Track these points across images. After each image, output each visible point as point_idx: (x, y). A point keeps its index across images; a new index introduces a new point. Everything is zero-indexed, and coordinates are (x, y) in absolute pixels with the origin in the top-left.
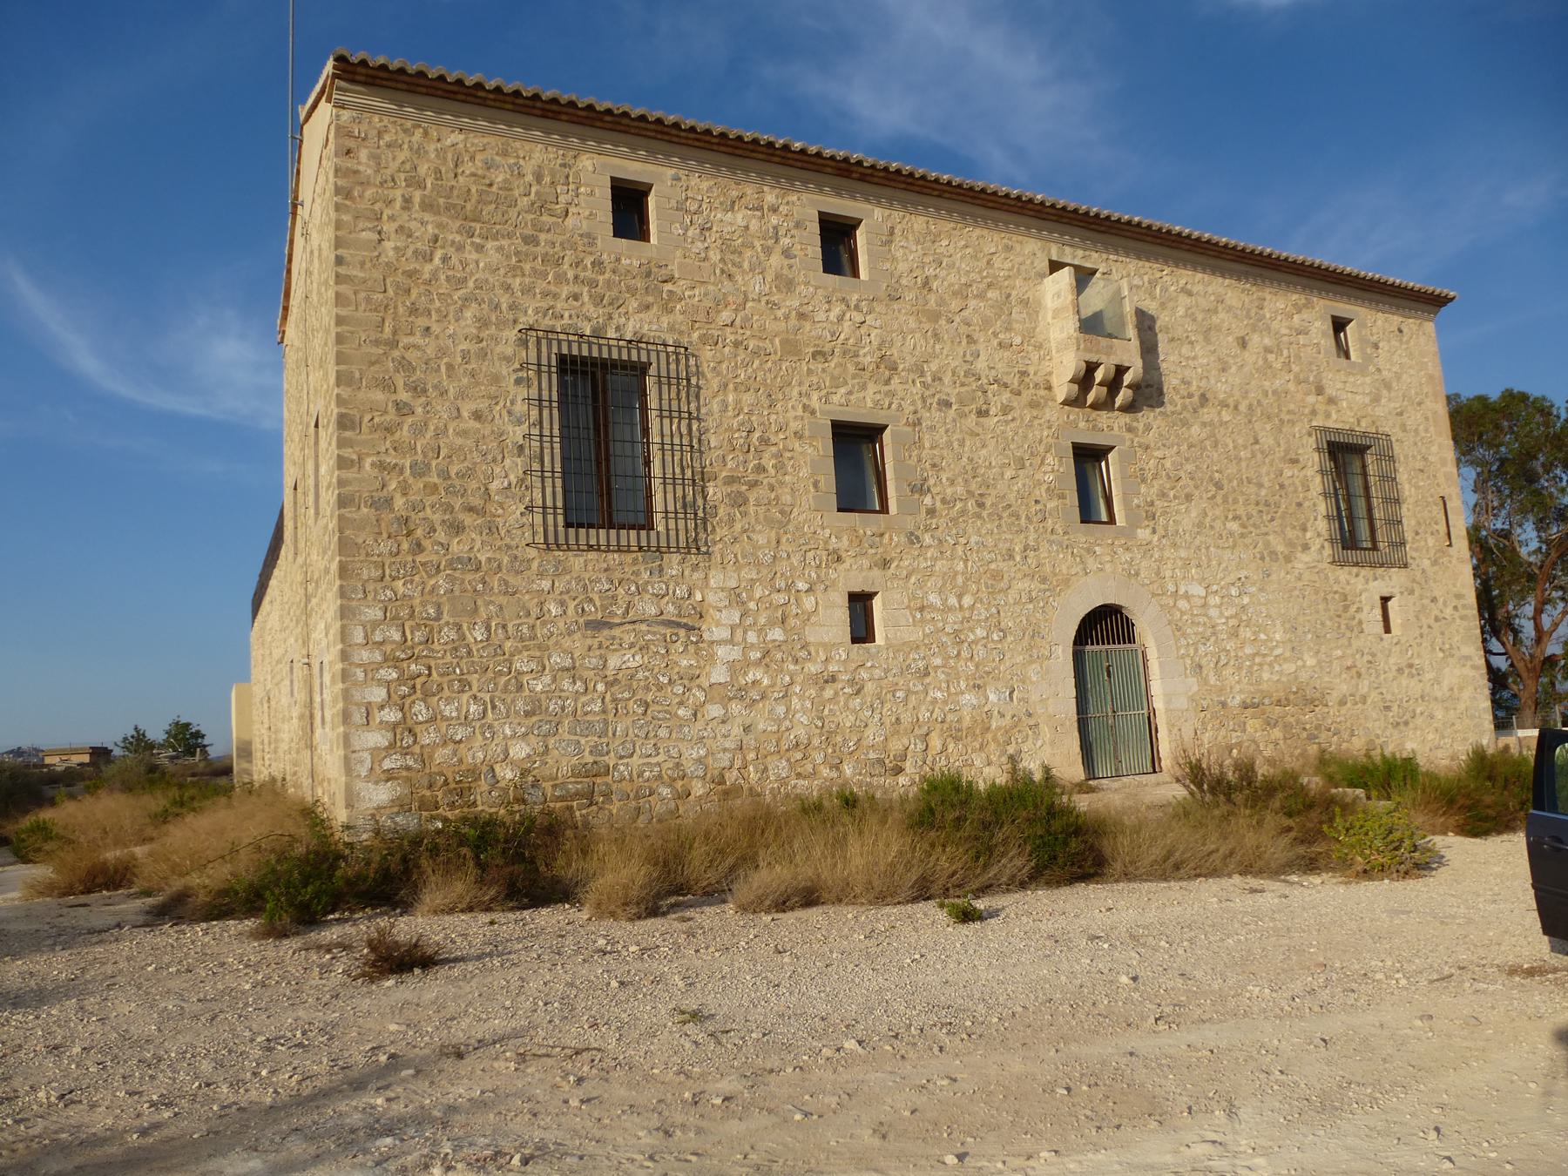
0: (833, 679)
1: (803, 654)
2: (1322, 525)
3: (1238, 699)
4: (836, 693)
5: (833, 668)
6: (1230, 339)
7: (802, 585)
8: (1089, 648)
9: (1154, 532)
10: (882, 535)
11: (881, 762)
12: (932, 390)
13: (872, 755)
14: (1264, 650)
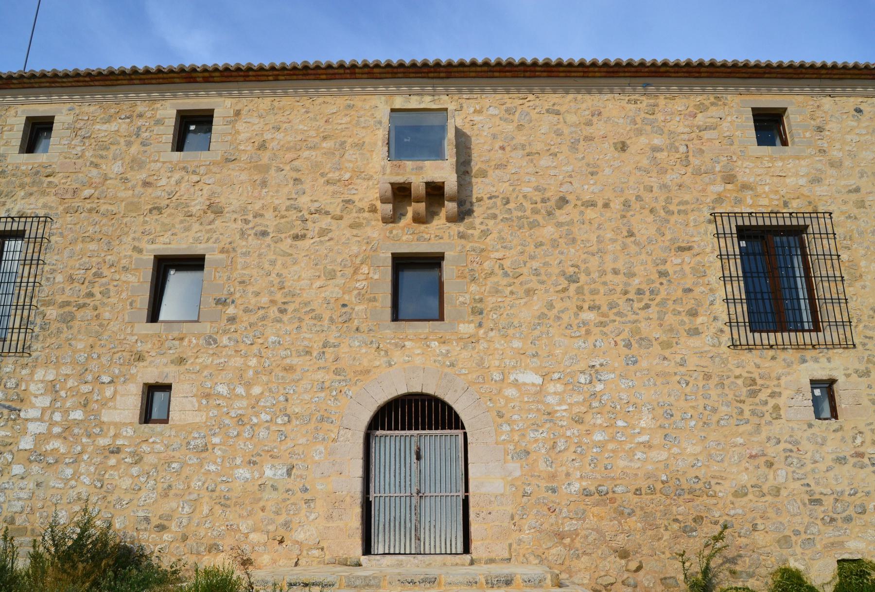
0: (117, 451)
1: (97, 430)
2: (721, 310)
3: (576, 486)
4: (118, 462)
5: (119, 442)
6: (606, 145)
7: (106, 379)
8: (379, 432)
9: (480, 325)
10: (182, 339)
11: (147, 519)
12: (251, 225)
13: (141, 514)
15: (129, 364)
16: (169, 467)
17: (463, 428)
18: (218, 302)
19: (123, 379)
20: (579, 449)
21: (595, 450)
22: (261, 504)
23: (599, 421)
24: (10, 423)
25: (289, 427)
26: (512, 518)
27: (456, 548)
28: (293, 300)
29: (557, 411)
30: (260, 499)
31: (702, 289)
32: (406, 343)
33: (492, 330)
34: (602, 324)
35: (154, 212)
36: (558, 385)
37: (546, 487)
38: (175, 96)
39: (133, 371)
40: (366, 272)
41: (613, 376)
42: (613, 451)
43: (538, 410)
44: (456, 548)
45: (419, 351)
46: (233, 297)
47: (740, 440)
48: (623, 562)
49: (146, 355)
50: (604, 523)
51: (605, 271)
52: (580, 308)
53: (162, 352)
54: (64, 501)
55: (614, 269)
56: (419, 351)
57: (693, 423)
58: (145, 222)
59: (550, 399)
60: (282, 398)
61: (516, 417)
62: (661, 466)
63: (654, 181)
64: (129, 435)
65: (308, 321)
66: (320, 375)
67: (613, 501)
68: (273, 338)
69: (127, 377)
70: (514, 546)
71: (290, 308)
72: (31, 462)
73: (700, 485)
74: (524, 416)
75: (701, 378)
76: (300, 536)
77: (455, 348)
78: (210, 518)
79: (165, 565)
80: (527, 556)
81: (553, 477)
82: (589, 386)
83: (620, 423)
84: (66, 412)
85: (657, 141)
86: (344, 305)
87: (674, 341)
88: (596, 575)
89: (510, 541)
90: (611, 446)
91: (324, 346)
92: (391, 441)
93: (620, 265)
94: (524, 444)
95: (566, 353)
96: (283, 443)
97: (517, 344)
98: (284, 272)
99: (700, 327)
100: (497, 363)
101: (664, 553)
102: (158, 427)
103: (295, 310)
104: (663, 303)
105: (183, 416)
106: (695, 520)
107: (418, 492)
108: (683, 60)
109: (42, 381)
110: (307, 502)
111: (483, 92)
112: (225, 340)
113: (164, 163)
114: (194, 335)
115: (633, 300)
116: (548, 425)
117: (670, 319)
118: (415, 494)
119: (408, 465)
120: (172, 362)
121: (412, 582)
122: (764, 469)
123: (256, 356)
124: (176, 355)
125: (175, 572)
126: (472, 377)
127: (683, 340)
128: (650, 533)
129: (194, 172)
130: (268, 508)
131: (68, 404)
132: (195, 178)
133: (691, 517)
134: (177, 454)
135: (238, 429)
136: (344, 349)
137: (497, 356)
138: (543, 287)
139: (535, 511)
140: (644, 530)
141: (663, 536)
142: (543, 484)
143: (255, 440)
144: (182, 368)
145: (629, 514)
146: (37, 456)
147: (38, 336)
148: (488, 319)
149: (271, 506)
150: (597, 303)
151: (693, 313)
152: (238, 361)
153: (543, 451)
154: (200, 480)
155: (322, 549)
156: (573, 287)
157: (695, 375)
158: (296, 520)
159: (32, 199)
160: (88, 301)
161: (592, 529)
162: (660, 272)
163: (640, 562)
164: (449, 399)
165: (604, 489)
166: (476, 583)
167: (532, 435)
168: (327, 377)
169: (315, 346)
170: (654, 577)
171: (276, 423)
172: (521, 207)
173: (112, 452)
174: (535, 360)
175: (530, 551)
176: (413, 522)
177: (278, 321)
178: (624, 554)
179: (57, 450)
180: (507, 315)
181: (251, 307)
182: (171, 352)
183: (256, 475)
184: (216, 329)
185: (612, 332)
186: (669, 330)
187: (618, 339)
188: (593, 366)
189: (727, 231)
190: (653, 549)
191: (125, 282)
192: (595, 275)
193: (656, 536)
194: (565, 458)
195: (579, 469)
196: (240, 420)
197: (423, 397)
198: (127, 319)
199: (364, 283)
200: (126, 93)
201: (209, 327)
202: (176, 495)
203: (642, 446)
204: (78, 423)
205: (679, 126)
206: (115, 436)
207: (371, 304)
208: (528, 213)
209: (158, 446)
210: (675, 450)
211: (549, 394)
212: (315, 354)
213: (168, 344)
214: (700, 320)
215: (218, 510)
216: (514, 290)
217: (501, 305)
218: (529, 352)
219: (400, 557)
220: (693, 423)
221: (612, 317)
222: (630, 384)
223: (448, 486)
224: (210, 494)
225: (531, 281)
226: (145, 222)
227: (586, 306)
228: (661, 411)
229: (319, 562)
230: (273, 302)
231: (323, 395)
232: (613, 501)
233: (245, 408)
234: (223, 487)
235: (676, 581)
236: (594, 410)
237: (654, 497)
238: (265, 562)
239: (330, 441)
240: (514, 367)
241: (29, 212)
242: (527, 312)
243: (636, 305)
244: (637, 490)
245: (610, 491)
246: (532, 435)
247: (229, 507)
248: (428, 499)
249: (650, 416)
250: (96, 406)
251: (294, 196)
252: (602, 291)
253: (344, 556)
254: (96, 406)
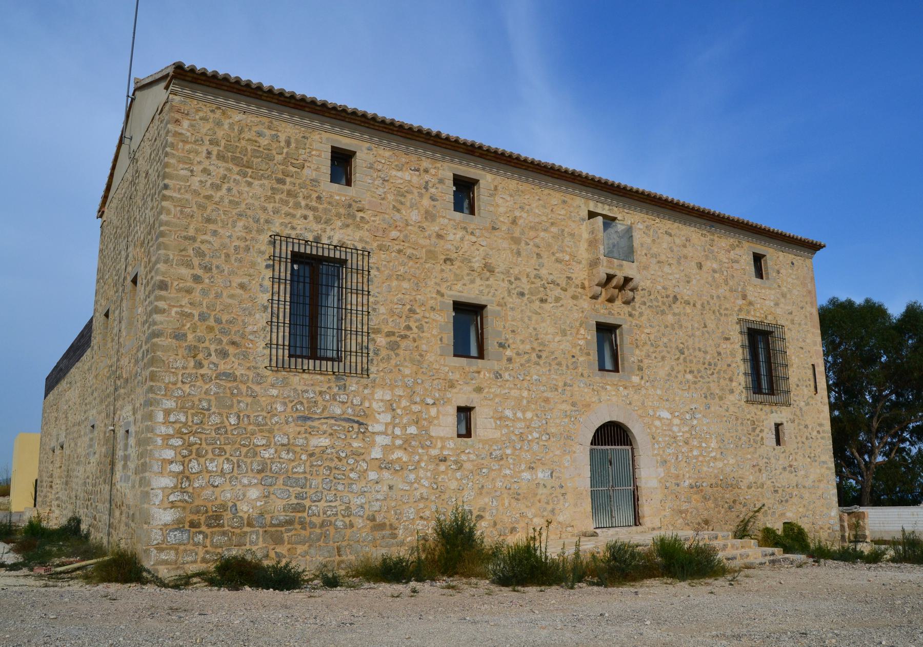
0: (444, 460)
3: (687, 483)
5: (446, 453)
10: (479, 372)
24: (361, 436)
35: (448, 262)
38: (452, 161)
39: (449, 395)
47: (749, 456)
54: (412, 500)
58: (442, 270)
60: (544, 422)
63: (714, 293)
68: (535, 377)
71: (544, 355)
72: (382, 469)
76: (561, 518)
77: (631, 391)
84: (404, 428)
85: (715, 266)
86: (573, 357)
97: (659, 392)
108: (434, 130)
109: (382, 401)
110: (563, 495)
111: (635, 210)
113: (450, 220)
122: (758, 474)
127: (727, 396)
129: (472, 233)
131: (405, 421)
132: (474, 239)
146: (384, 465)
147: (372, 360)
152: (515, 393)
156: (682, 357)
159: (349, 231)
160: (408, 333)
172: (656, 299)
173: (441, 461)
179: (399, 459)
189: (284, 255)
196: (521, 437)
200: (416, 148)
204: (413, 437)
205: (723, 256)
206: (443, 448)
208: (660, 304)
210: (725, 462)
212: (560, 390)
219: (617, 529)
226: (442, 270)
230: (533, 349)
231: (566, 420)
241: (349, 244)
250: (425, 423)
251: (537, 267)
254: (425, 423)
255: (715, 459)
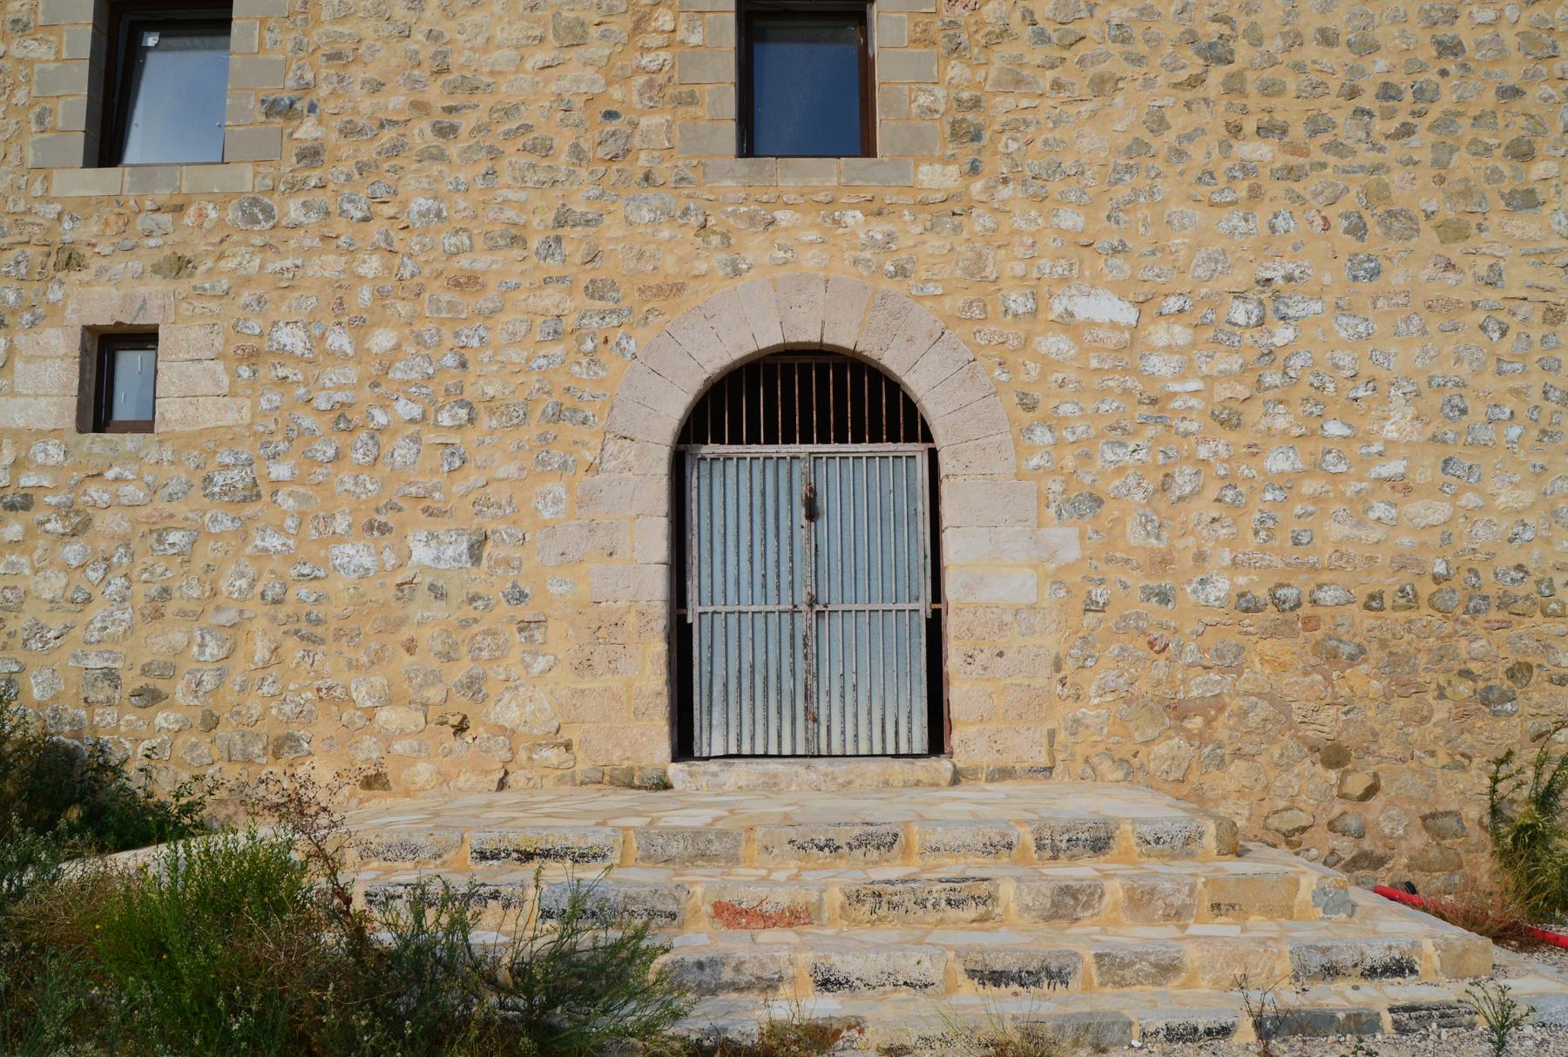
3: (1221, 587)
4: (28, 531)
5: (28, 480)
9: (974, 169)
10: (179, 209)
11: (111, 676)
13: (95, 662)
14: (1332, 463)
15: (44, 278)
16: (160, 541)
17: (928, 437)
18: (273, 108)
19: (27, 317)
20: (1230, 493)
21: (1269, 496)
22: (405, 633)
23: (1281, 423)
25: (472, 435)
26: (1058, 667)
27: (910, 741)
28: (474, 100)
29: (1175, 394)
30: (401, 622)
31: (1546, 89)
32: (779, 214)
33: (1005, 181)
34: (1292, 173)
36: (1177, 329)
37: (1144, 589)
39: (55, 294)
40: (669, 26)
41: (1317, 307)
42: (1315, 499)
43: (1126, 392)
44: (910, 741)
45: (813, 235)
46: (314, 98)
48: (1333, 775)
49: (88, 252)
50: (1288, 678)
51: (1298, 35)
52: (1236, 130)
53: (128, 244)
55: (1322, 31)
56: (813, 235)
57: (1515, 432)
59: (1158, 365)
60: (450, 360)
61: (1067, 409)
62: (1434, 538)
64: (51, 462)
65: (513, 157)
66: (550, 299)
67: (1311, 623)
68: (420, 203)
69: (39, 311)
70: (1062, 736)
71: (466, 122)
73: (1528, 587)
74: (1090, 408)
75: (1537, 318)
76: (509, 714)
77: (909, 228)
78: (275, 671)
79: (163, 790)
80: (1095, 760)
81: (1164, 561)
82: (1256, 332)
83: (1334, 428)
86: (610, 115)
87: (1473, 221)
88: (1266, 807)
89: (1051, 725)
90: (1309, 487)
91: (560, 223)
92: (741, 474)
93: (1338, 21)
94: (1088, 480)
95: (1199, 245)
96: (457, 475)
97: (1070, 219)
98: (448, 28)
99: (1539, 188)
100: (1019, 269)
101: (1432, 754)
102: (129, 441)
103: (478, 129)
104: (1446, 123)
105: (191, 410)
106: (1511, 674)
107: (813, 601)
110: (524, 626)
112: (293, 210)
114: (212, 197)
115: (1370, 114)
116: (1150, 431)
117: (1464, 164)
118: (803, 607)
119: (784, 534)
120: (156, 269)
121: (831, 847)
123: (377, 249)
124: (167, 252)
125: (188, 809)
126: (950, 304)
127: (1494, 219)
128: (1400, 704)
130: (422, 645)
133: (1502, 667)
134: (179, 509)
135: (339, 440)
136: (612, 228)
137: (1019, 252)
138: (1138, 72)
139: (1115, 649)
140: (1387, 697)
141: (1431, 711)
142: (1137, 580)
143: (383, 469)
144: (183, 286)
145: (1352, 658)
148: (995, 153)
149: (430, 639)
150: (1279, 117)
151: (1523, 153)
152: (329, 265)
153: (1138, 497)
154: (242, 575)
155: (568, 746)
156: (1217, 74)
157: (1524, 309)
158: (497, 672)
161: (1259, 695)
162: (1439, 43)
163: (1375, 775)
164: (893, 360)
165: (1290, 593)
166: (1009, 846)
167: (1110, 456)
168: (569, 304)
169: (535, 221)
170: (1406, 813)
171: (437, 425)
173: (12, 507)
174: (1118, 261)
175: (1101, 748)
176: (800, 676)
177: (433, 158)
178: (1335, 757)
180: (1046, 142)
181: (361, 122)
182: (152, 242)
183: (390, 559)
184: (269, 182)
185: (1316, 195)
186: (1460, 194)
187: (1330, 212)
188: (1268, 280)
190: (1408, 745)
191: (20, 60)
192: (1274, 45)
193: (1415, 711)
194: (1194, 516)
195: (1229, 542)
197: (822, 360)
198: (30, 160)
199: (663, 55)
201: (249, 176)
202: (183, 614)
203: (1387, 486)
207: (681, 111)
209: (131, 488)
210: (1470, 499)
211: (1153, 350)
212: (534, 244)
213: (143, 222)
214: (1538, 169)
215: (294, 650)
216: (1064, 79)
217: (1029, 116)
218: (1103, 243)
220: (1515, 432)
221: (1318, 155)
222: (1361, 328)
223: (890, 586)
224: (271, 609)
225: (1109, 55)
227: (1250, 125)
228: (1435, 400)
229: (561, 780)
230: (420, 107)
231: (558, 350)
232: (1311, 623)
233: (354, 387)
234: (303, 593)
235: (1459, 821)
236: (1270, 395)
237: (1413, 615)
238: (420, 780)
239: (581, 472)
240: (1064, 280)
242: (1095, 139)
243: (1379, 126)
244: (1372, 597)
245: (1305, 599)
246: (1110, 456)
247: (322, 641)
248: (837, 620)
249: (1410, 412)
252: (1292, 87)
253: (626, 764)
255: (1402, 487)
